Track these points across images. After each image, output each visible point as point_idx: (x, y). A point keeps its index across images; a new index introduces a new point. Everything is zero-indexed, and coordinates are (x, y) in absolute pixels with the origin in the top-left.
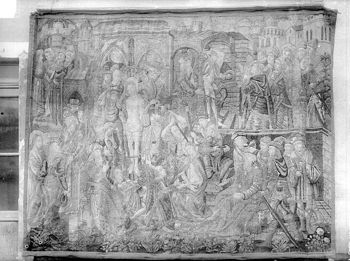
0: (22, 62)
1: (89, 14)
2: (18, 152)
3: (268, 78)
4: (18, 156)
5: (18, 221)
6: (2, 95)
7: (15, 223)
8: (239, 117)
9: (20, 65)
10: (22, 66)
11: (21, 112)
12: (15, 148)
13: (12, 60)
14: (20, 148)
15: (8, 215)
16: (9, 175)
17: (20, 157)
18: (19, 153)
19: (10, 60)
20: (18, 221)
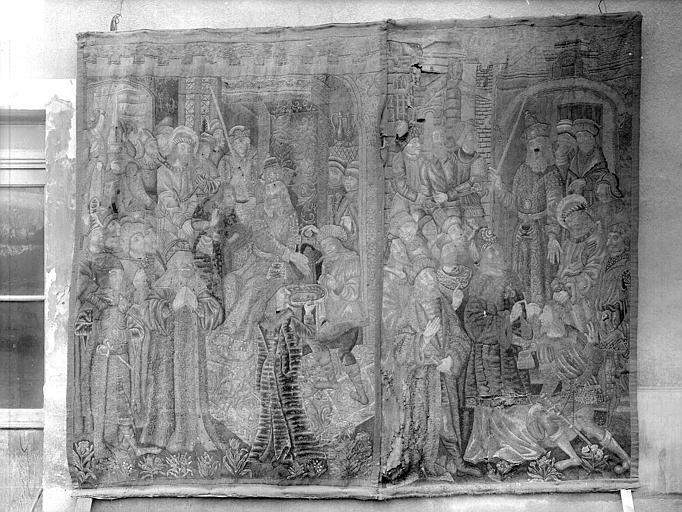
0: (51, 118)
1: (457, 495)
2: (42, 293)
3: (247, 140)
4: (43, 301)
5: (42, 429)
6: (6, 182)
7: (37, 432)
8: (449, 434)
9: (48, 123)
10: (50, 125)
11: (49, 216)
12: (37, 285)
13: (26, 115)
14: (47, 285)
15: (24, 416)
16: (29, 336)
17: (47, 304)
18: (45, 297)
19: (20, 114)
20: (42, 429)
